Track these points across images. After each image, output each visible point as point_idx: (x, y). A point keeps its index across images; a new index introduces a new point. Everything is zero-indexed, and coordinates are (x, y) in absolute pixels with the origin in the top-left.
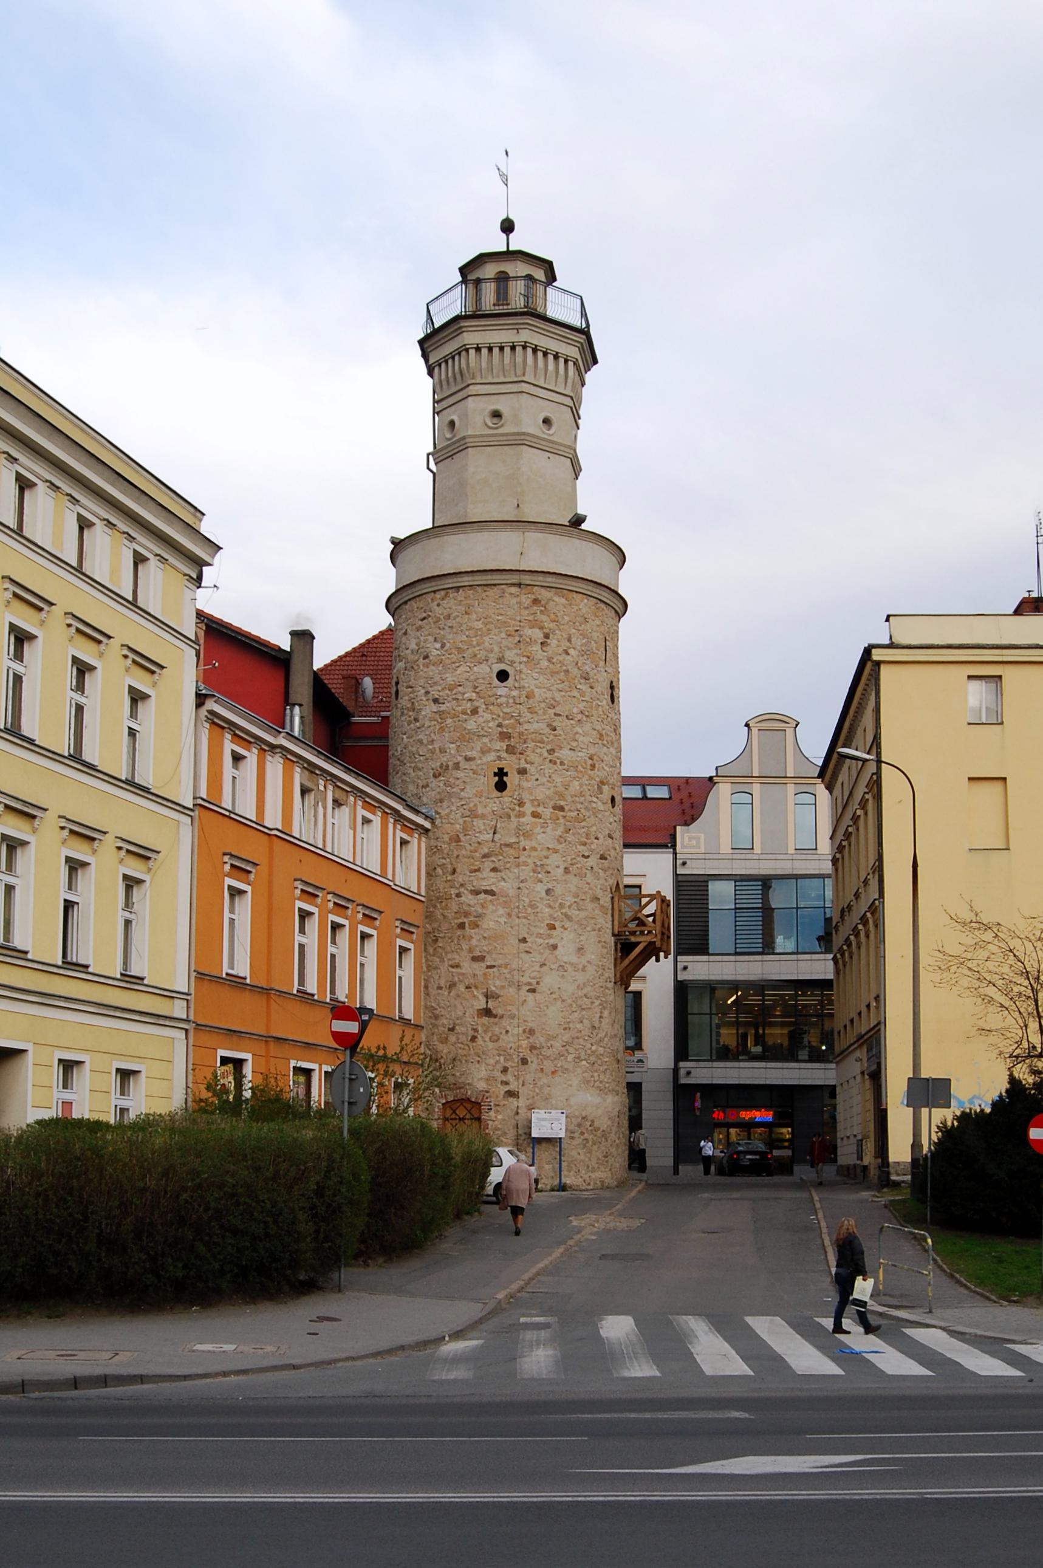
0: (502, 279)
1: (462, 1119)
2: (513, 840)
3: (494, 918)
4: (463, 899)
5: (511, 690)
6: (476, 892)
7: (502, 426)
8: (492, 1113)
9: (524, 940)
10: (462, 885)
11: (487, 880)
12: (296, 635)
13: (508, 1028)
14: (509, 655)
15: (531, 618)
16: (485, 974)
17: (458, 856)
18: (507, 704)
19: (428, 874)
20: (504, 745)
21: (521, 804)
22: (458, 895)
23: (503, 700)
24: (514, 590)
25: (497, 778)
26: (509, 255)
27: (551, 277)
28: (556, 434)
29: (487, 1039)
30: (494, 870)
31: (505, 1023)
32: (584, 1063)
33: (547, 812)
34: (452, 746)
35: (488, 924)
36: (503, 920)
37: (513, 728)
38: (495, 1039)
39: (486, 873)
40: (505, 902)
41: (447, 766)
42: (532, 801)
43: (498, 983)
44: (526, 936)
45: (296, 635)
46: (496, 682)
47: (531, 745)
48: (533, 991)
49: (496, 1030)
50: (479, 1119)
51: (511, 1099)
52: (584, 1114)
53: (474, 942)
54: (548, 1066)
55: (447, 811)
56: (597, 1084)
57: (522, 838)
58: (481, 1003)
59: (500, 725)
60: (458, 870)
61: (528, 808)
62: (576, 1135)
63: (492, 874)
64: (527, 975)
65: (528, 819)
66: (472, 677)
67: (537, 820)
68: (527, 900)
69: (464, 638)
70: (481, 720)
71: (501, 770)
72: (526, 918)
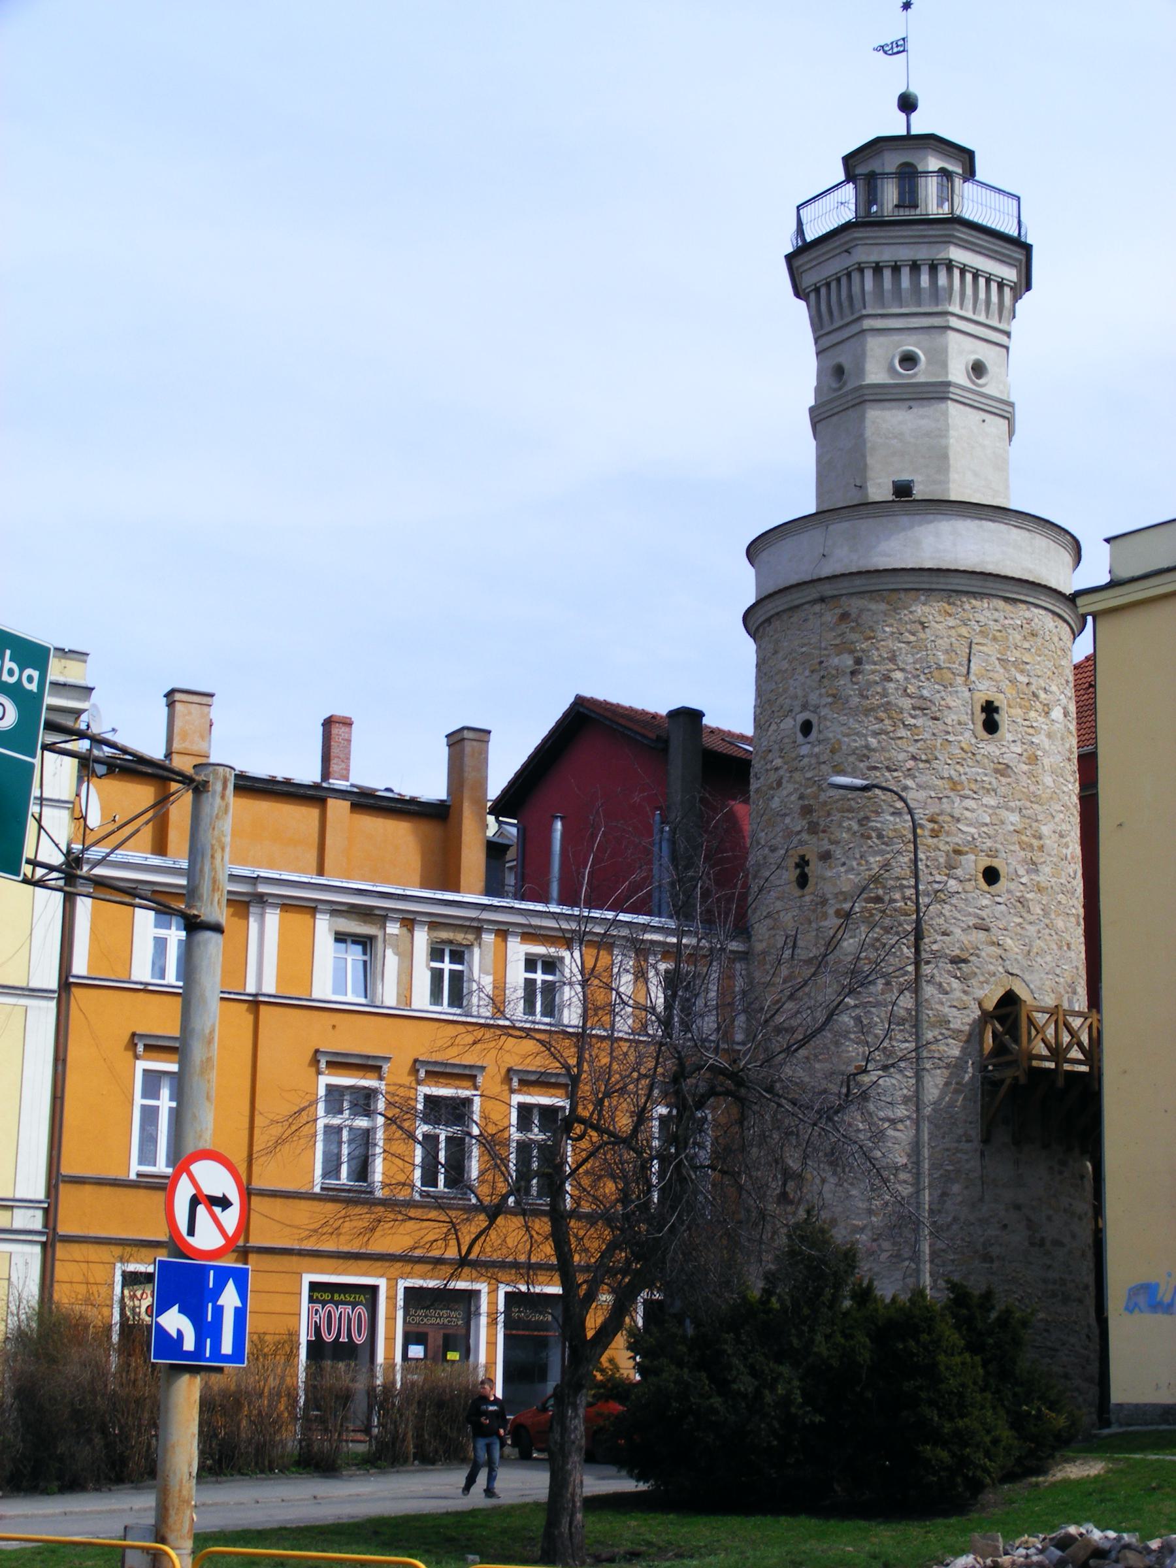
0: (909, 176)
5: (814, 746)
14: (813, 698)
15: (838, 642)
21: (824, 902)
23: (806, 760)
24: (817, 608)
25: (798, 871)
27: (970, 173)
28: (990, 386)
37: (816, 797)
47: (837, 816)
59: (801, 797)
70: (785, 793)
71: (802, 857)
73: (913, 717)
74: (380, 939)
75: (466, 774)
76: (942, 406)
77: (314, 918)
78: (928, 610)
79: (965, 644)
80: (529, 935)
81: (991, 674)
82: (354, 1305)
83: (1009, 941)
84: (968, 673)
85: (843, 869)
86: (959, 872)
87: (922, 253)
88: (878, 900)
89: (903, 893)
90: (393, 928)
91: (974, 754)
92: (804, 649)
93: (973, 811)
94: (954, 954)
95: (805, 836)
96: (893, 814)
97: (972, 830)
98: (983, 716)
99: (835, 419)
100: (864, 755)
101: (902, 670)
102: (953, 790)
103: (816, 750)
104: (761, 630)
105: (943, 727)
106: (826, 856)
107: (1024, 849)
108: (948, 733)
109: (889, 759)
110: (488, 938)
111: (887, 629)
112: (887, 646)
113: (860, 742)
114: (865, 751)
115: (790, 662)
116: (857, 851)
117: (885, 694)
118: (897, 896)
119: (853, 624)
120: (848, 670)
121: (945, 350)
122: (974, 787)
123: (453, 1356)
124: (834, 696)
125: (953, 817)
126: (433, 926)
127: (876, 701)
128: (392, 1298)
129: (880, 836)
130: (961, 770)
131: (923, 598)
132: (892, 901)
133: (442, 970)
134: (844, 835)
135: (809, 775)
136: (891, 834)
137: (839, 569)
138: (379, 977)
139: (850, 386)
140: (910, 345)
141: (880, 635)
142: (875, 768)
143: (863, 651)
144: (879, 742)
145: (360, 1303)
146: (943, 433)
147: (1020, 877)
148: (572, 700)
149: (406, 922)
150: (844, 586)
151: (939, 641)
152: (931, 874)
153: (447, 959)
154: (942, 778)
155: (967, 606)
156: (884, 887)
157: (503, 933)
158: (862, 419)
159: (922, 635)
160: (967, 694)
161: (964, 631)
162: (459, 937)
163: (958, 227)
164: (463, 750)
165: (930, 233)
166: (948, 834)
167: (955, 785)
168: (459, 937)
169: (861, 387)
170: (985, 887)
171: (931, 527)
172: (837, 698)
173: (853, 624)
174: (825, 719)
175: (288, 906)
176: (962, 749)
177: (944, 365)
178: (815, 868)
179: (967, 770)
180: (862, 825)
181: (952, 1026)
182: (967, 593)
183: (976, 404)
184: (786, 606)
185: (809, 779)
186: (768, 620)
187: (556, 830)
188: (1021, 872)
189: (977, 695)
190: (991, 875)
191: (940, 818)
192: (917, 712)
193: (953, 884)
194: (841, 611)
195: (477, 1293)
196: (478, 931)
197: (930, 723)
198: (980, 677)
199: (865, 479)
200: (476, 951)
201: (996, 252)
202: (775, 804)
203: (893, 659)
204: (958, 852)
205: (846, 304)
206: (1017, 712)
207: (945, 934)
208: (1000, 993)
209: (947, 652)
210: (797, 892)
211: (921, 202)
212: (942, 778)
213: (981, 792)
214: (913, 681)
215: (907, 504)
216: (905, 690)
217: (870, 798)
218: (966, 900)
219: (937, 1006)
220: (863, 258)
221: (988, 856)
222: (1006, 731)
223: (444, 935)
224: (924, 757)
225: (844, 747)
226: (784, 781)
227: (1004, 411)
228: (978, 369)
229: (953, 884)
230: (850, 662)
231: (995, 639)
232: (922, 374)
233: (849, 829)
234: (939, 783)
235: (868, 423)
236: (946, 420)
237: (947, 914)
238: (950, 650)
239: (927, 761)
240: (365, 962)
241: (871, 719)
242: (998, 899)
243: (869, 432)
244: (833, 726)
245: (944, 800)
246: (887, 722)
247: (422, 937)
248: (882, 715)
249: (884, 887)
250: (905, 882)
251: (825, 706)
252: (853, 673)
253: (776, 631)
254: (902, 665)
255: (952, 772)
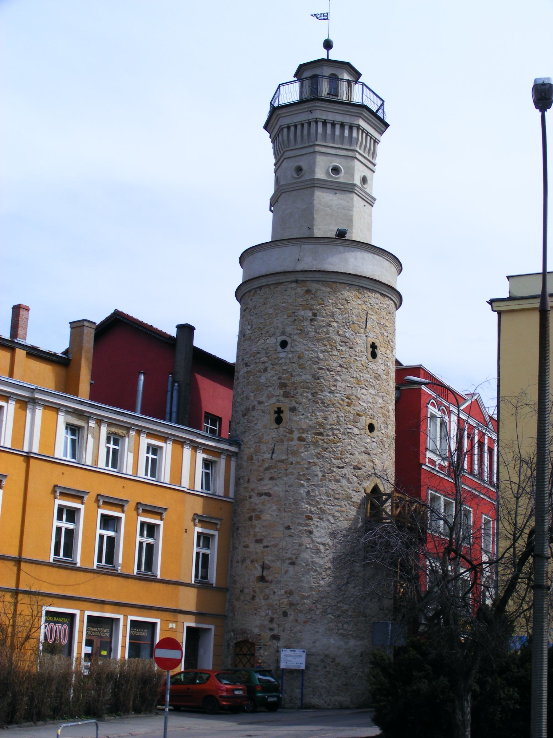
1: (245, 655)
2: (284, 457)
3: (270, 513)
4: (253, 500)
5: (288, 353)
6: (260, 495)
7: (302, 176)
8: (262, 651)
9: (288, 528)
10: (252, 490)
11: (267, 486)
12: (180, 328)
13: (276, 590)
14: (289, 330)
15: (304, 303)
16: (262, 552)
17: (251, 470)
18: (286, 363)
19: (237, 484)
20: (282, 392)
21: (291, 432)
22: (250, 497)
23: (283, 361)
24: (293, 285)
25: (276, 415)
26: (326, 62)
29: (262, 598)
30: (271, 478)
31: (273, 586)
32: (330, 616)
33: (309, 437)
34: (252, 394)
35: (266, 517)
36: (275, 514)
38: (266, 598)
39: (266, 481)
40: (278, 501)
41: (249, 409)
42: (299, 429)
43: (270, 558)
44: (290, 524)
45: (180, 328)
46: (279, 349)
48: (293, 563)
49: (267, 591)
50: (253, 655)
51: (274, 641)
52: (326, 653)
53: (257, 530)
54: (302, 618)
55: (247, 440)
56: (340, 631)
57: (290, 456)
58: (258, 573)
59: (280, 378)
60: (251, 480)
61: (296, 435)
62: (320, 668)
63: (270, 482)
64: (289, 552)
65: (296, 442)
66: (265, 347)
67: (302, 443)
68: (292, 499)
69: (263, 321)
70: (269, 375)
71: (279, 409)
72: (290, 511)
73: (341, 346)
74: (86, 428)
75: (84, 344)
76: (351, 195)
77: (57, 414)
78: (349, 294)
79: (365, 313)
80: (151, 434)
81: (375, 330)
82: (63, 623)
83: (377, 461)
84: (366, 328)
85: (302, 417)
86: (358, 424)
87: (347, 119)
88: (321, 434)
89: (333, 432)
90: (92, 424)
91: (367, 368)
92: (284, 305)
93: (365, 395)
94: (355, 464)
95: (281, 398)
96: (330, 392)
97: (365, 405)
98: (371, 350)
99: (294, 193)
100: (316, 362)
101: (337, 322)
102: (358, 384)
103: (290, 356)
104: (253, 292)
105: (354, 353)
106: (293, 410)
107: (383, 417)
108: (356, 356)
109: (329, 365)
110: (133, 433)
111: (330, 301)
112: (330, 309)
113: (314, 355)
114: (317, 360)
115: (275, 310)
116: (310, 409)
117: (328, 333)
118: (330, 433)
119: (312, 296)
120: (309, 318)
121: (353, 169)
122: (366, 384)
123: (104, 653)
124: (301, 330)
125: (357, 397)
126: (110, 425)
127: (323, 335)
128: (82, 621)
129: (323, 403)
130: (361, 374)
131: (348, 288)
132: (328, 435)
133: (109, 448)
134: (304, 400)
135: (285, 368)
136: (329, 402)
137: (306, 268)
138: (84, 449)
139: (306, 177)
140: (337, 162)
141: (326, 303)
142: (322, 369)
143: (318, 310)
144: (324, 356)
145: (65, 623)
146: (350, 208)
147: (382, 430)
148: (112, 311)
149: (98, 421)
150: (310, 276)
151: (354, 310)
152: (346, 424)
153: (112, 442)
154: (353, 378)
155: (366, 295)
156: (324, 428)
157: (139, 432)
158: (312, 195)
159: (347, 306)
160: (365, 338)
161: (364, 307)
162: (120, 432)
163: (365, 110)
164: (82, 332)
165: (352, 110)
166: (355, 405)
167: (358, 382)
168: (120, 432)
169: (314, 179)
170: (369, 433)
171: (353, 254)
172: (302, 332)
173: (312, 296)
174: (296, 341)
175: (48, 406)
176: (362, 364)
177: (353, 175)
178: (286, 415)
179: (364, 375)
180: (314, 396)
181: (353, 500)
182: (366, 288)
183: (363, 197)
184: (274, 282)
185: (285, 370)
186: (260, 288)
187: (141, 379)
188: (382, 428)
189: (369, 339)
190: (371, 428)
191: (351, 397)
192: (343, 344)
193: (356, 431)
194: (306, 288)
195: (118, 620)
196: (128, 429)
197: (349, 350)
198: (370, 330)
199: (312, 225)
200: (127, 439)
201: (375, 125)
202: (263, 380)
203: (332, 316)
204: (358, 415)
205: (305, 136)
206: (383, 349)
207: (351, 454)
208: (373, 485)
209: (357, 316)
210: (276, 426)
211: (339, 95)
212: (353, 378)
213: (369, 386)
214: (342, 328)
215: (343, 241)
216: (338, 332)
217: (318, 383)
218: (361, 438)
219: (347, 490)
220: (319, 116)
221: (370, 418)
222: (380, 359)
223: (114, 430)
224: (345, 366)
225: (306, 356)
226: (269, 369)
227: (370, 201)
228: (364, 180)
229: (356, 431)
230: (310, 314)
231: (376, 313)
232: (342, 178)
233: (307, 397)
234: (352, 380)
235: (315, 198)
236: (352, 203)
237: (353, 444)
238: (358, 316)
239: (346, 368)
240: (73, 441)
241: (320, 344)
242: (374, 440)
243: (316, 202)
244: (300, 345)
245: (354, 388)
246: (328, 346)
247: (104, 430)
248: (326, 343)
249: (324, 428)
250: (334, 427)
251: (295, 334)
252: (311, 320)
253: (265, 293)
254: (337, 320)
255: (358, 375)
